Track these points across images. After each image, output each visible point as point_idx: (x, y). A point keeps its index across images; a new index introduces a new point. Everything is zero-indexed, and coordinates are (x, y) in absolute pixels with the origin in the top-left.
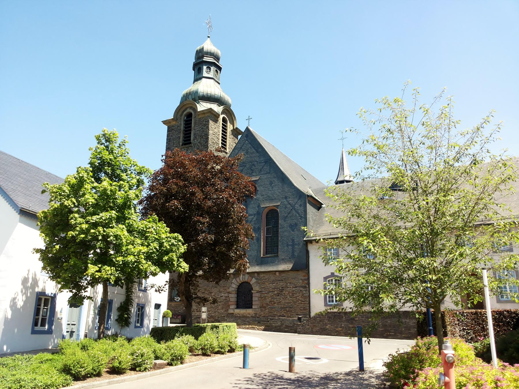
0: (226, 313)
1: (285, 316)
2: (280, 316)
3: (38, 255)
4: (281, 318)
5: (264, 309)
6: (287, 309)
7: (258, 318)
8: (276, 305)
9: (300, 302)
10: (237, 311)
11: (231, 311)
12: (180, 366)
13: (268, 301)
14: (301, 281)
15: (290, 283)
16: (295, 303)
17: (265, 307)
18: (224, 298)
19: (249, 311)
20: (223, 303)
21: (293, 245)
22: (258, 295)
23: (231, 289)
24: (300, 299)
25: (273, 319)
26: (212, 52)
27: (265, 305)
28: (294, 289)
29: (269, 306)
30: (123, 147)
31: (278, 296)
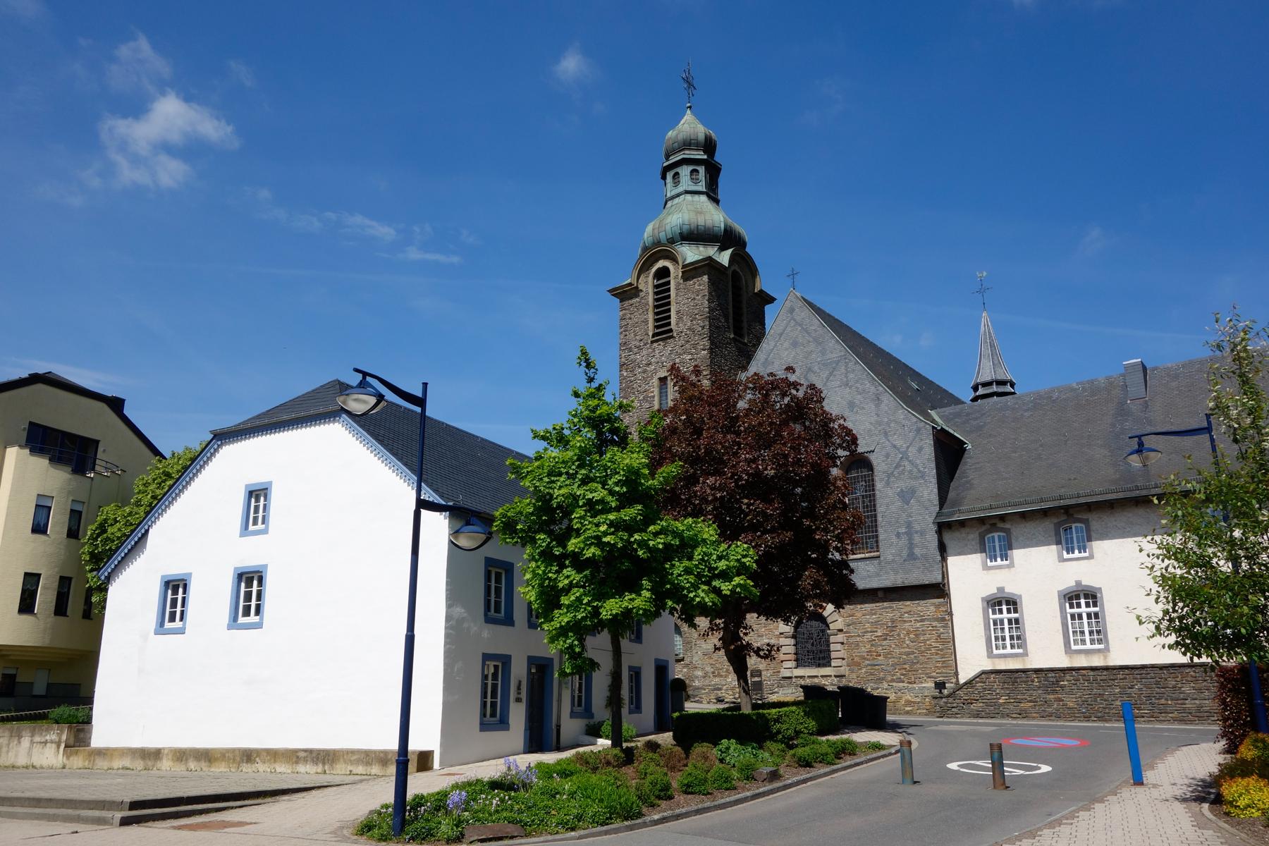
2: (893, 681)
17: (859, 664)
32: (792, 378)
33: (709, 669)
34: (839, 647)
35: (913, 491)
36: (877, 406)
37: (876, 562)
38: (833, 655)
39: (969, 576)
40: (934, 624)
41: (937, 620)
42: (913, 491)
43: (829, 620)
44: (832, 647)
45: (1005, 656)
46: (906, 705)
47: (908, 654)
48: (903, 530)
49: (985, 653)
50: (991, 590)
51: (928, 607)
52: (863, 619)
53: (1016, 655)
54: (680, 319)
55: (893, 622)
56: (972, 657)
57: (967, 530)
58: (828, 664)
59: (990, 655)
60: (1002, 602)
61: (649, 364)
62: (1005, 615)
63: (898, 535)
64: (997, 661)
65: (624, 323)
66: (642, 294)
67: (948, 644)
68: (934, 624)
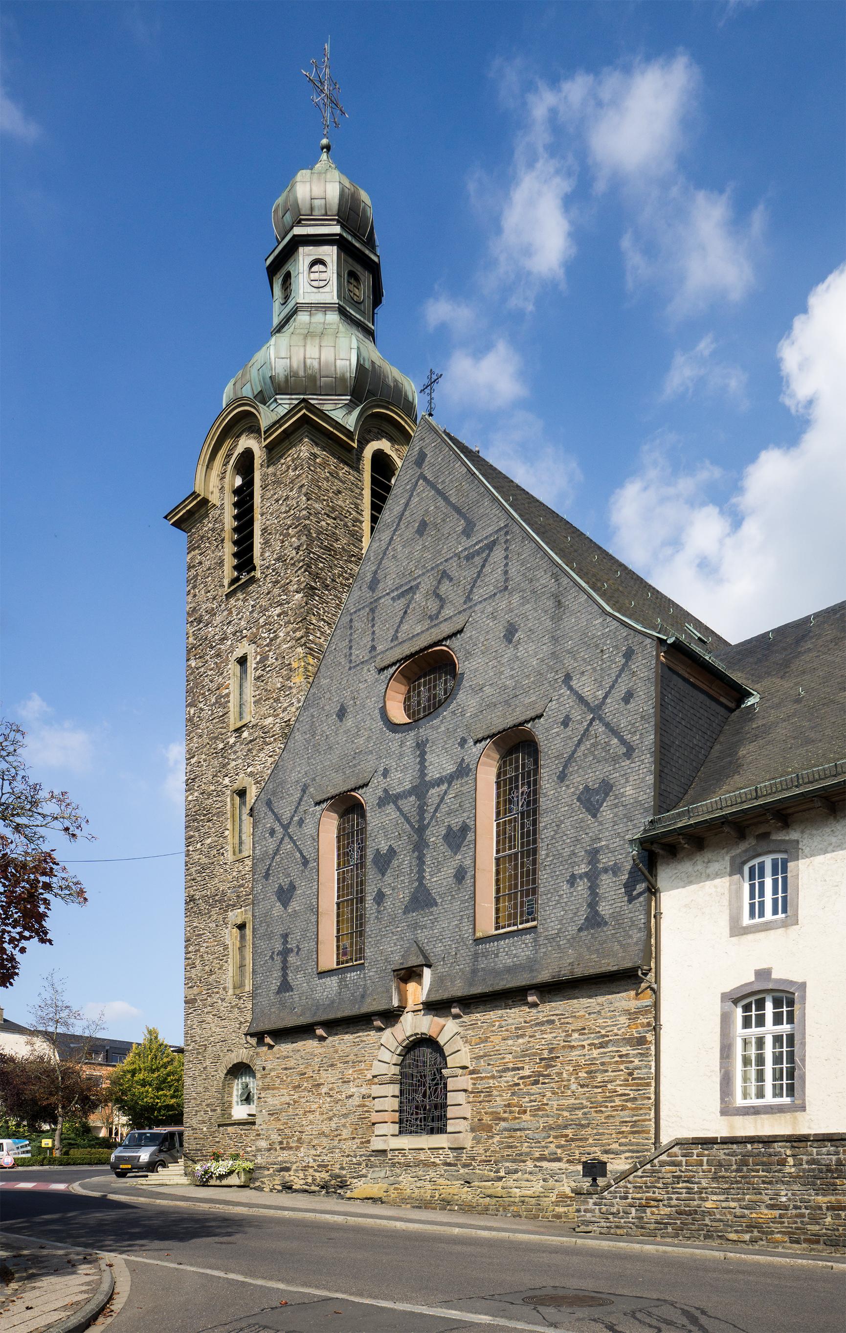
0: (363, 1151)
1: (559, 1160)
2: (542, 1158)
3: (47, 995)
4: (545, 1164)
5: (484, 1135)
6: (569, 1132)
7: (465, 1166)
8: (526, 1117)
9: (618, 1102)
10: (406, 1142)
11: (377, 1144)
12: (727, 989)
13: (500, 1102)
14: (623, 1020)
15: (581, 1031)
16: (597, 1107)
17: (489, 1128)
18: (356, 1101)
19: (440, 1140)
20: (352, 1118)
21: (593, 877)
22: (465, 1081)
23: (379, 1068)
24: (620, 1090)
25: (516, 1171)
26: (798, 323)
27: (487, 1119)
28: (595, 1053)
29: (503, 1124)
30: (550, 604)
31: (536, 1082)
32: (83, 825)
33: (276, 1137)
34: (461, 1098)
35: (606, 787)
36: (557, 619)
37: (528, 938)
38: (451, 1112)
39: (702, 931)
40: (624, 1050)
41: (629, 1041)
42: (606, 787)
43: (447, 1050)
44: (451, 1098)
45: (755, 1111)
46: (556, 1204)
47: (573, 1109)
48: (583, 868)
49: (717, 1105)
50: (743, 977)
51: (615, 1008)
52: (502, 1046)
53: (780, 1109)
54: (266, 543)
55: (551, 1050)
56: (691, 1102)
57: (708, 855)
58: (442, 1130)
59: (727, 1110)
60: (770, 1000)
61: (223, 639)
62: (770, 1028)
63: (572, 881)
64: (738, 1120)
65: (193, 572)
66: (213, 513)
67: (646, 1088)
68: (624, 1050)
